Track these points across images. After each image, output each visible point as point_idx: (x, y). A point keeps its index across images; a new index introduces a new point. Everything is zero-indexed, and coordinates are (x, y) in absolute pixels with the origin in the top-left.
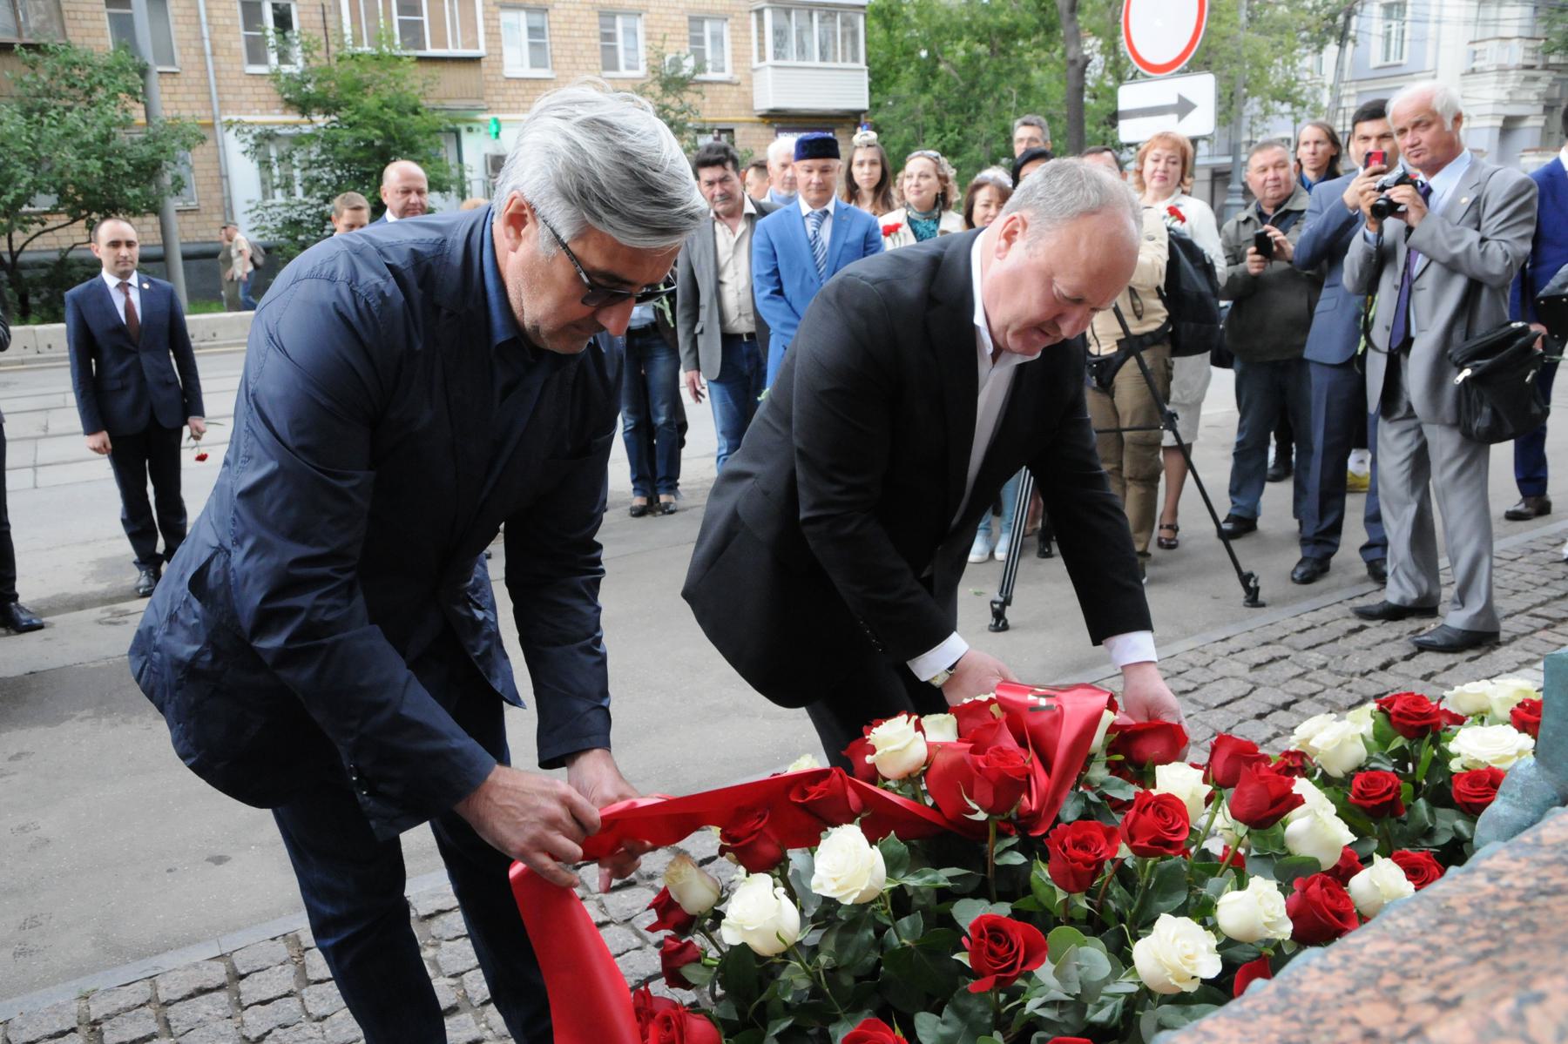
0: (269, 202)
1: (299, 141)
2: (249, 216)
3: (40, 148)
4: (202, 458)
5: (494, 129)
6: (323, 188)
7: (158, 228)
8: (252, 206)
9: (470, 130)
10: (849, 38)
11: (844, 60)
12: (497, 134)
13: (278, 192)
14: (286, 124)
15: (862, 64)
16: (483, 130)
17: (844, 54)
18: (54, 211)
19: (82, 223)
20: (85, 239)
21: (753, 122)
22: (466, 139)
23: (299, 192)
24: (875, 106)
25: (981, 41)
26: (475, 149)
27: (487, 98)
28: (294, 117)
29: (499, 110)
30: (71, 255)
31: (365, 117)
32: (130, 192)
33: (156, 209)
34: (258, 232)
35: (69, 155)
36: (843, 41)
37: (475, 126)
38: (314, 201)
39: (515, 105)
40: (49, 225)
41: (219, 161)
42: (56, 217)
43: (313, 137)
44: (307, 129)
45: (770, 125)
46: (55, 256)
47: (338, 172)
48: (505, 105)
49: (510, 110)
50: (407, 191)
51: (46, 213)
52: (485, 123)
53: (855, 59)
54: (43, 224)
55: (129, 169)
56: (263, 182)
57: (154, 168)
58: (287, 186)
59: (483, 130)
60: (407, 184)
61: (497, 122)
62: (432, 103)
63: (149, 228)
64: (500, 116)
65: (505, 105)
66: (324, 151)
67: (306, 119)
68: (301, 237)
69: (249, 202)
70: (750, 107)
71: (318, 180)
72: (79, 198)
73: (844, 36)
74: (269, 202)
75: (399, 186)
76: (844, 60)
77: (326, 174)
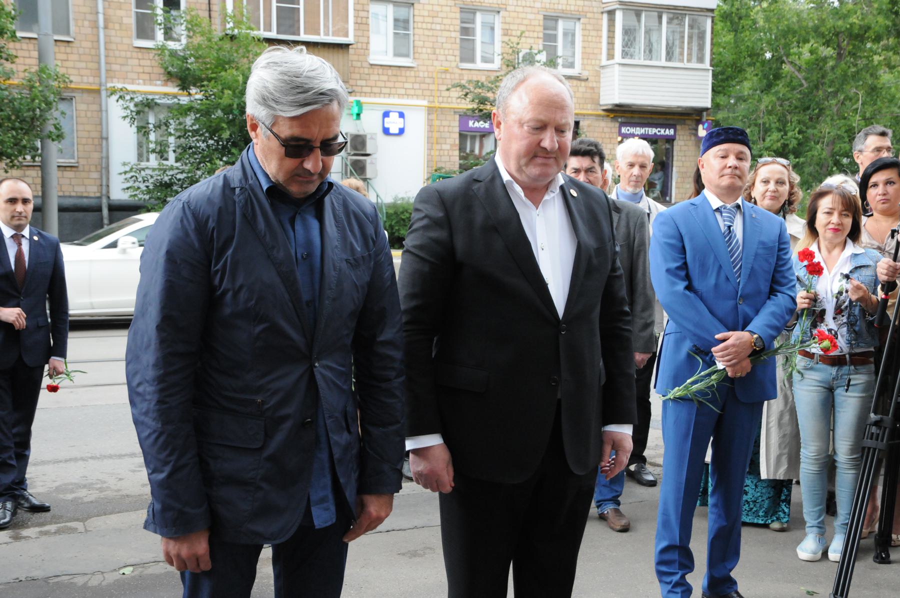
0: (144, 164)
2: (123, 176)
5: (355, 110)
7: (39, 181)
8: (127, 168)
10: (695, 39)
11: (689, 61)
12: (358, 115)
15: (707, 64)
17: (690, 54)
24: (716, 106)
25: (827, 44)
36: (690, 43)
39: (384, 90)
41: (101, 124)
45: (614, 119)
48: (368, 90)
53: (701, 60)
61: (359, 104)
64: (363, 99)
65: (368, 90)
69: (124, 164)
73: (690, 37)
74: (144, 164)
76: (689, 61)
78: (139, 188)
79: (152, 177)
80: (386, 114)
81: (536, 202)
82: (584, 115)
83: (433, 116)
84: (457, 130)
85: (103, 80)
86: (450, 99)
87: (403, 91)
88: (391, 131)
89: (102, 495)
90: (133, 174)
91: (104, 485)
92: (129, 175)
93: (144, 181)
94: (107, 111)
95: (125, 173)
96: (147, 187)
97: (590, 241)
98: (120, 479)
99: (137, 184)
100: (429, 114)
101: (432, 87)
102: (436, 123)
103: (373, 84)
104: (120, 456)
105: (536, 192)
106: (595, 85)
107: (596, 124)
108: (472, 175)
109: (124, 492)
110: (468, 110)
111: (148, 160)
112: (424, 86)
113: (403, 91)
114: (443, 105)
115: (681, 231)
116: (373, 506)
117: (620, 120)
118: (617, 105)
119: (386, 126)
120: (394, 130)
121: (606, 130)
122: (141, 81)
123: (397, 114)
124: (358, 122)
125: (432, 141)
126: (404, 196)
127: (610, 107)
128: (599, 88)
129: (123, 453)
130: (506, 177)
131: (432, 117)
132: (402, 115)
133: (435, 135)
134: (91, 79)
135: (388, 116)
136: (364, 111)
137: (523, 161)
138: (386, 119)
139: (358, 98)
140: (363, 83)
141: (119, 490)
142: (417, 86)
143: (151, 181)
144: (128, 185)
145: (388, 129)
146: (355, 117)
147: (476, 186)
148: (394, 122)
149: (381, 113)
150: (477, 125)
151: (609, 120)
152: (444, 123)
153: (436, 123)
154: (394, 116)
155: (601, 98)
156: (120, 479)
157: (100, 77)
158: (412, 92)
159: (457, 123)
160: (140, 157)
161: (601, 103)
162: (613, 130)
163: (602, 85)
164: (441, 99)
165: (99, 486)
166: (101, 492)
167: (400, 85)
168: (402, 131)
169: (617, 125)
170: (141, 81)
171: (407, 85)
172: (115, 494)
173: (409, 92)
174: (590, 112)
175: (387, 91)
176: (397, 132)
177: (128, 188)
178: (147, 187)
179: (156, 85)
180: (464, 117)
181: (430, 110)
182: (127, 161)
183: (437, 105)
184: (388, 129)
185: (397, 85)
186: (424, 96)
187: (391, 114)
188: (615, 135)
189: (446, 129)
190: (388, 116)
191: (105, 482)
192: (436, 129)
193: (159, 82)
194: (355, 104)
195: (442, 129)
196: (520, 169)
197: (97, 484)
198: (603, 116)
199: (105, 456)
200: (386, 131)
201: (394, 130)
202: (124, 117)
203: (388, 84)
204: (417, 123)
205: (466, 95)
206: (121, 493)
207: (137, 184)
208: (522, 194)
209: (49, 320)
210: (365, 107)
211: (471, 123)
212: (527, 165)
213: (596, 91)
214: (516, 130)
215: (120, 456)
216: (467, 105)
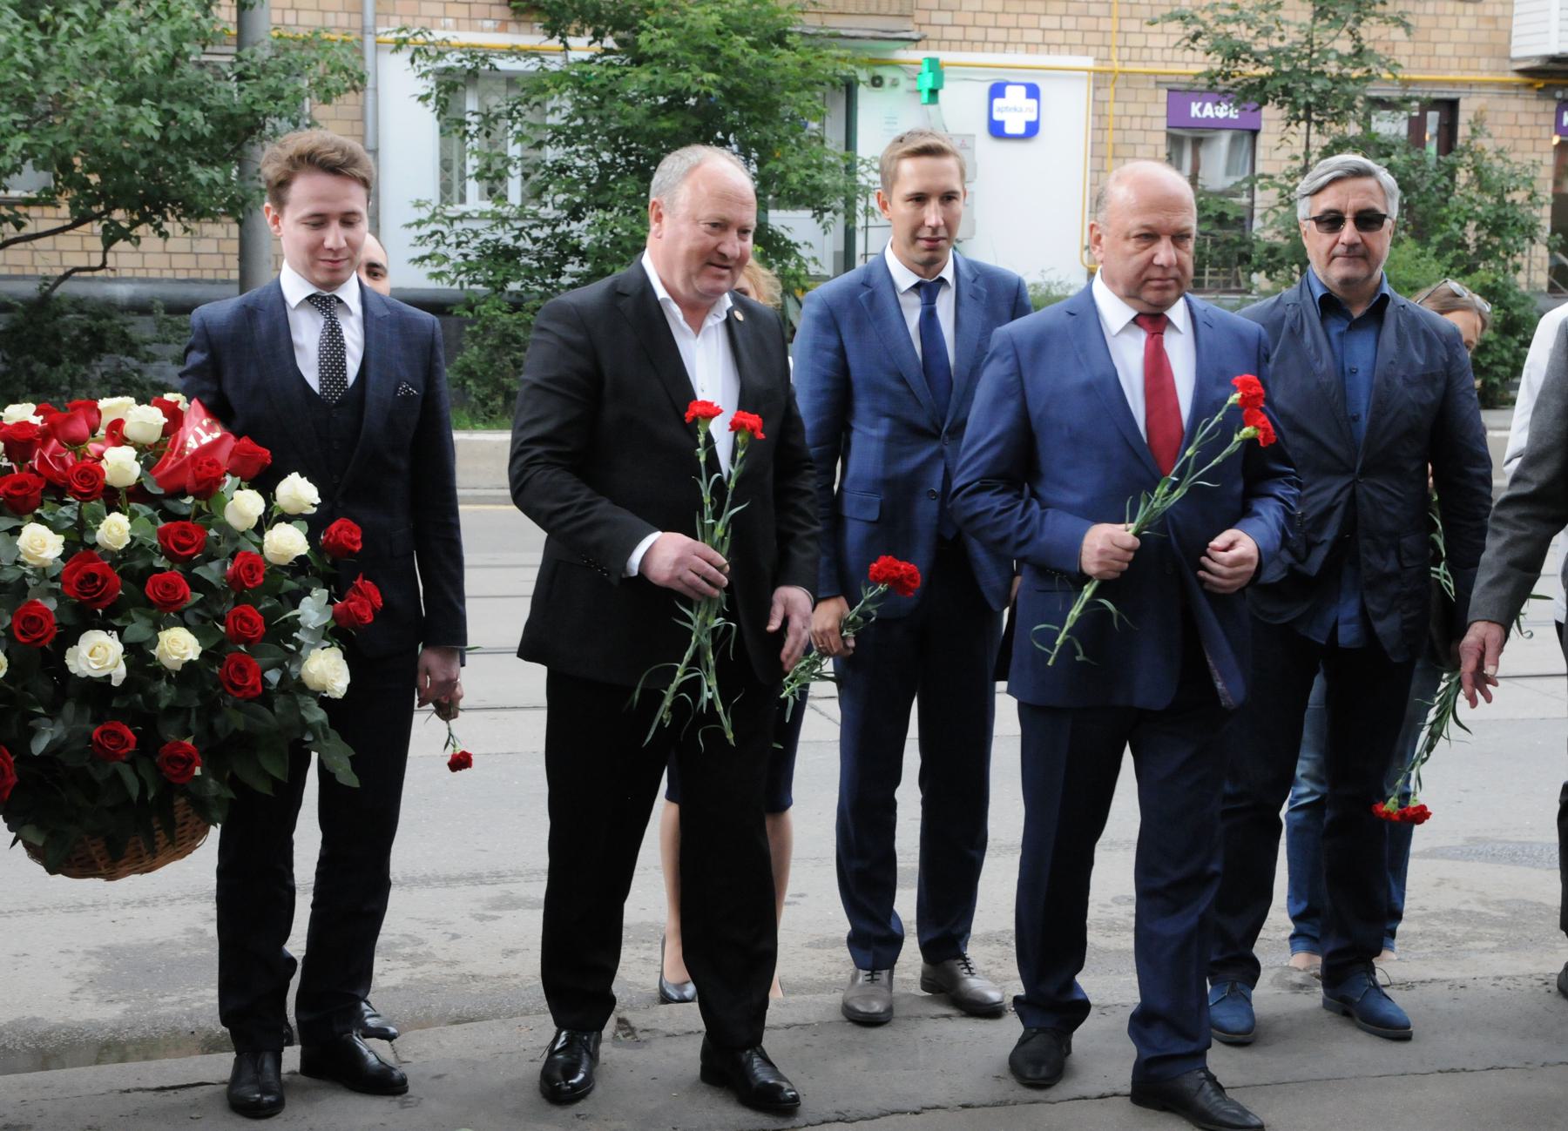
0: (455, 210)
1: (535, 88)
2: (414, 231)
3: (48, 77)
4: (460, 762)
5: (927, 82)
6: (571, 187)
7: (234, 246)
8: (425, 214)
9: (877, 82)
12: (934, 92)
13: (473, 188)
14: (513, 52)
16: (904, 84)
18: (46, 199)
19: (96, 227)
20: (96, 261)
21: (1506, 85)
22: (869, 103)
23: (515, 189)
26: (881, 120)
27: (920, 17)
28: (533, 38)
29: (950, 44)
30: (66, 288)
31: (683, 43)
32: (202, 175)
33: (239, 209)
34: (430, 267)
35: (99, 99)
37: (887, 74)
38: (548, 212)
39: (994, 34)
40: (30, 229)
41: (363, 119)
42: (49, 211)
43: (561, 79)
44: (555, 64)
45: (1545, 93)
46: (30, 289)
47: (606, 157)
48: (956, 33)
49: (966, 43)
50: (1150, 236)
51: (28, 203)
52: (911, 69)
54: (19, 225)
55: (207, 130)
56: (446, 166)
57: (251, 131)
58: (493, 179)
59: (904, 84)
60: (1151, 220)
61: (936, 67)
62: (811, 22)
63: (210, 246)
64: (944, 56)
65: (956, 33)
66: (581, 110)
67: (555, 43)
68: (514, 286)
69: (418, 205)
70: (1502, 52)
71: (562, 169)
72: (94, 179)
74: (455, 210)
75: (1134, 223)
77: (582, 160)
78: (446, 258)
79: (476, 234)
80: (997, 91)
81: (697, 326)
82: (1470, 84)
83: (1107, 94)
84: (1162, 124)
85: (369, 21)
86: (1146, 53)
87: (1036, 36)
88: (1008, 130)
89: (418, 973)
90: (433, 227)
91: (421, 950)
92: (426, 230)
93: (459, 245)
94: (376, 89)
95: (419, 223)
96: (465, 256)
97: (758, 380)
98: (455, 937)
99: (442, 249)
100: (1096, 88)
101: (1104, 24)
102: (1114, 109)
103: (969, 20)
104: (449, 881)
105: (696, 310)
106: (1499, 10)
107: (1501, 104)
108: (613, 286)
109: (467, 968)
110: (1197, 76)
111: (463, 200)
112: (1086, 23)
113: (1036, 36)
114: (1129, 67)
115: (854, 361)
116: (895, 928)
117: (1559, 94)
118: (1553, 59)
119: (997, 117)
120: (1015, 126)
121: (1523, 119)
122: (450, 21)
123: (1023, 90)
124: (932, 108)
125: (1106, 150)
126: (1039, 280)
127: (1535, 64)
128: (1511, 17)
129: (454, 873)
130: (661, 293)
131: (1101, 95)
132: (1033, 92)
133: (1111, 137)
134: (343, 20)
135: (1002, 95)
136: (946, 84)
137: (694, 268)
138: (997, 102)
139: (933, 54)
140: (946, 18)
141: (452, 963)
142: (1069, 23)
143: (475, 243)
144: (426, 250)
145: (1001, 124)
146: (925, 96)
147: (622, 303)
148: (1015, 111)
149: (986, 87)
150: (1209, 111)
151: (1532, 94)
152: (1133, 109)
153: (1114, 109)
154: (1016, 95)
155: (1515, 42)
156: (455, 937)
157: (362, 13)
158: (1058, 37)
159: (1162, 110)
160: (446, 188)
161: (1515, 54)
162: (1542, 120)
163: (1517, 10)
164: (1125, 53)
165: (408, 950)
166: (415, 965)
167: (1033, 21)
168: (1032, 129)
169: (1552, 106)
170: (450, 21)
171: (1046, 22)
172: (446, 970)
173: (1050, 37)
174: (1486, 77)
175: (1000, 35)
176: (1021, 130)
177: (422, 259)
178: (465, 256)
179: (482, 30)
180: (1179, 95)
181: (1100, 79)
182: (424, 198)
183: (1117, 66)
184: (1001, 124)
185: (1024, 21)
186: (1085, 48)
187: (1009, 89)
188: (1545, 132)
189: (1137, 123)
190: (1002, 95)
191: (421, 942)
192: (1112, 122)
193: (488, 24)
194: (925, 68)
195: (1126, 123)
196: (688, 279)
197: (404, 945)
198: (1517, 87)
199: (413, 880)
200: (997, 130)
201: (1015, 126)
202: (424, 98)
203: (1003, 20)
204: (1068, 110)
205: (1195, 38)
206: (458, 969)
207: (442, 249)
208: (681, 317)
209: (730, 736)
210: (948, 74)
211: (1195, 109)
212: (698, 275)
213: (1502, 24)
214: (685, 228)
215: (449, 881)
216: (1197, 63)
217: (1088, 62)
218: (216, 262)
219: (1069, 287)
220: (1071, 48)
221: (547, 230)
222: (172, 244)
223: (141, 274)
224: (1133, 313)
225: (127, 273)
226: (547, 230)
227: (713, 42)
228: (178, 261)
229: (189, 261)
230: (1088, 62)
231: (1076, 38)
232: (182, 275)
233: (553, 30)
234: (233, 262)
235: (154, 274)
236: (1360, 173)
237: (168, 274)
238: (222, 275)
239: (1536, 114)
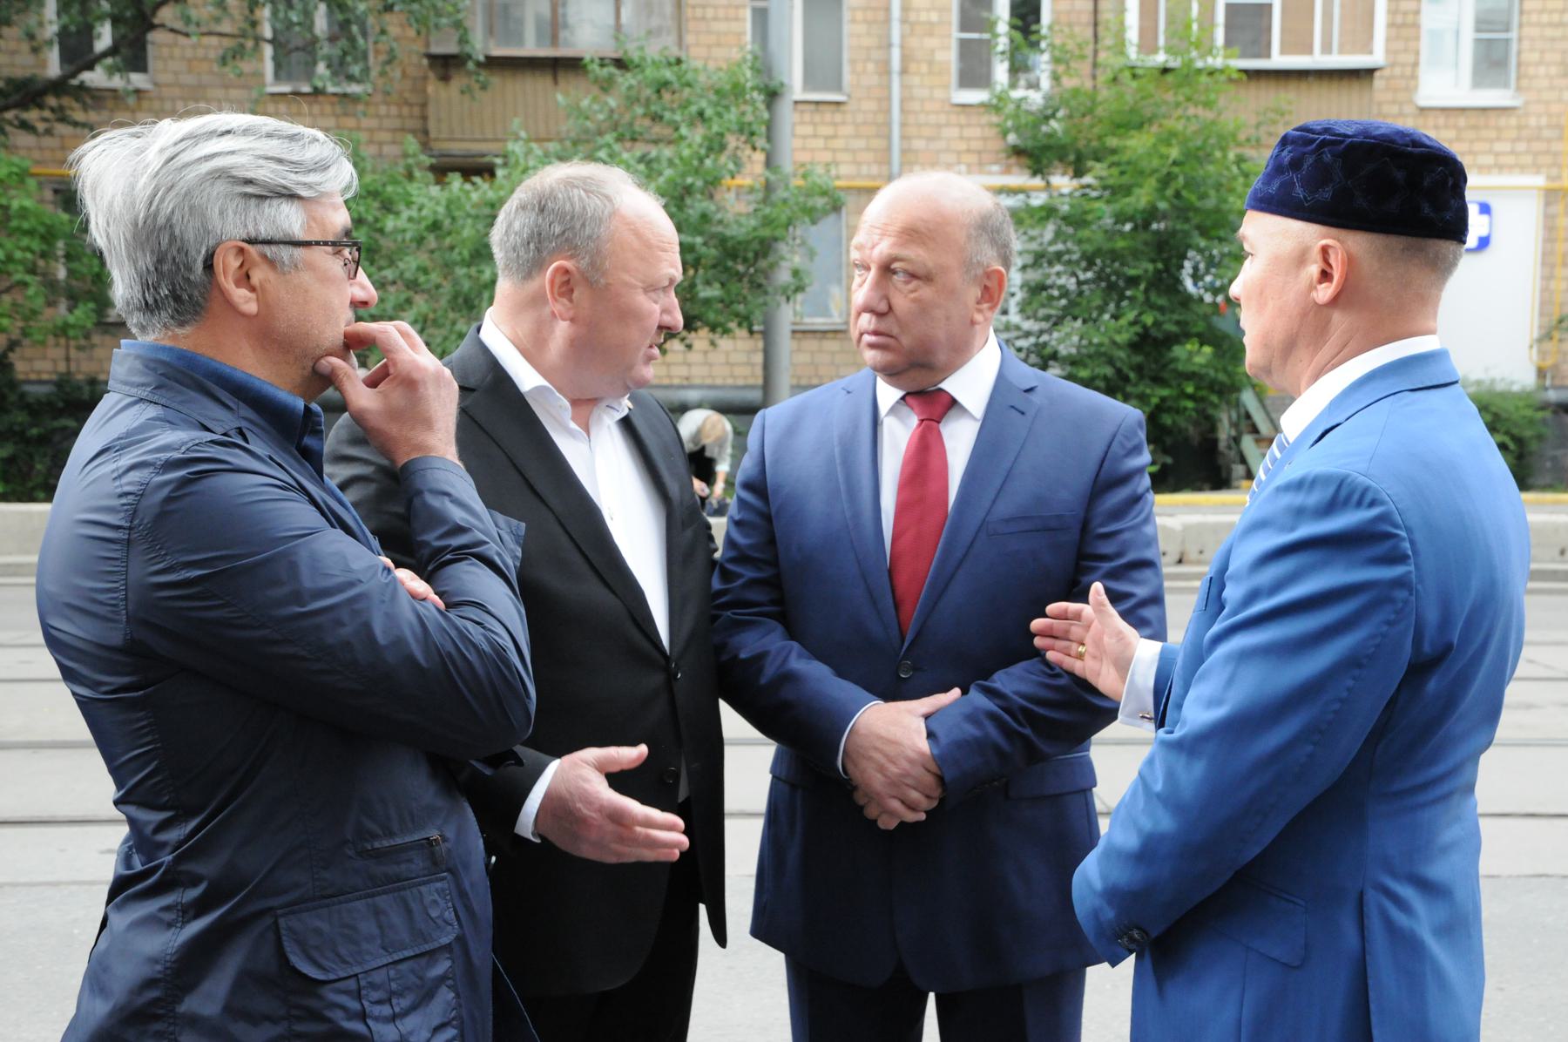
44: (1038, 200)
67: (1038, 182)
87: (1489, 160)
100: (1547, 204)
112: (1538, 146)
113: (1489, 160)
142: (1521, 146)
158: (1510, 160)
167: (1486, 146)
171: (1498, 147)
179: (990, 173)
181: (1551, 196)
185: (1478, 146)
186: (1536, 168)
193: (995, 168)
217: (1540, 181)
218: (746, 371)
219: (1512, 383)
220: (1523, 168)
221: (1032, 340)
222: (694, 357)
223: (708, 381)
224: (899, 394)
225: (697, 381)
226: (1032, 340)
227: (460, 115)
228: (738, 371)
229: (704, 371)
230: (1540, 181)
231: (1528, 159)
232: (741, 382)
233: (1037, 171)
234: (759, 371)
235: (719, 382)
236: (38, 163)
237: (730, 381)
238: (751, 381)
239: (961, 126)
